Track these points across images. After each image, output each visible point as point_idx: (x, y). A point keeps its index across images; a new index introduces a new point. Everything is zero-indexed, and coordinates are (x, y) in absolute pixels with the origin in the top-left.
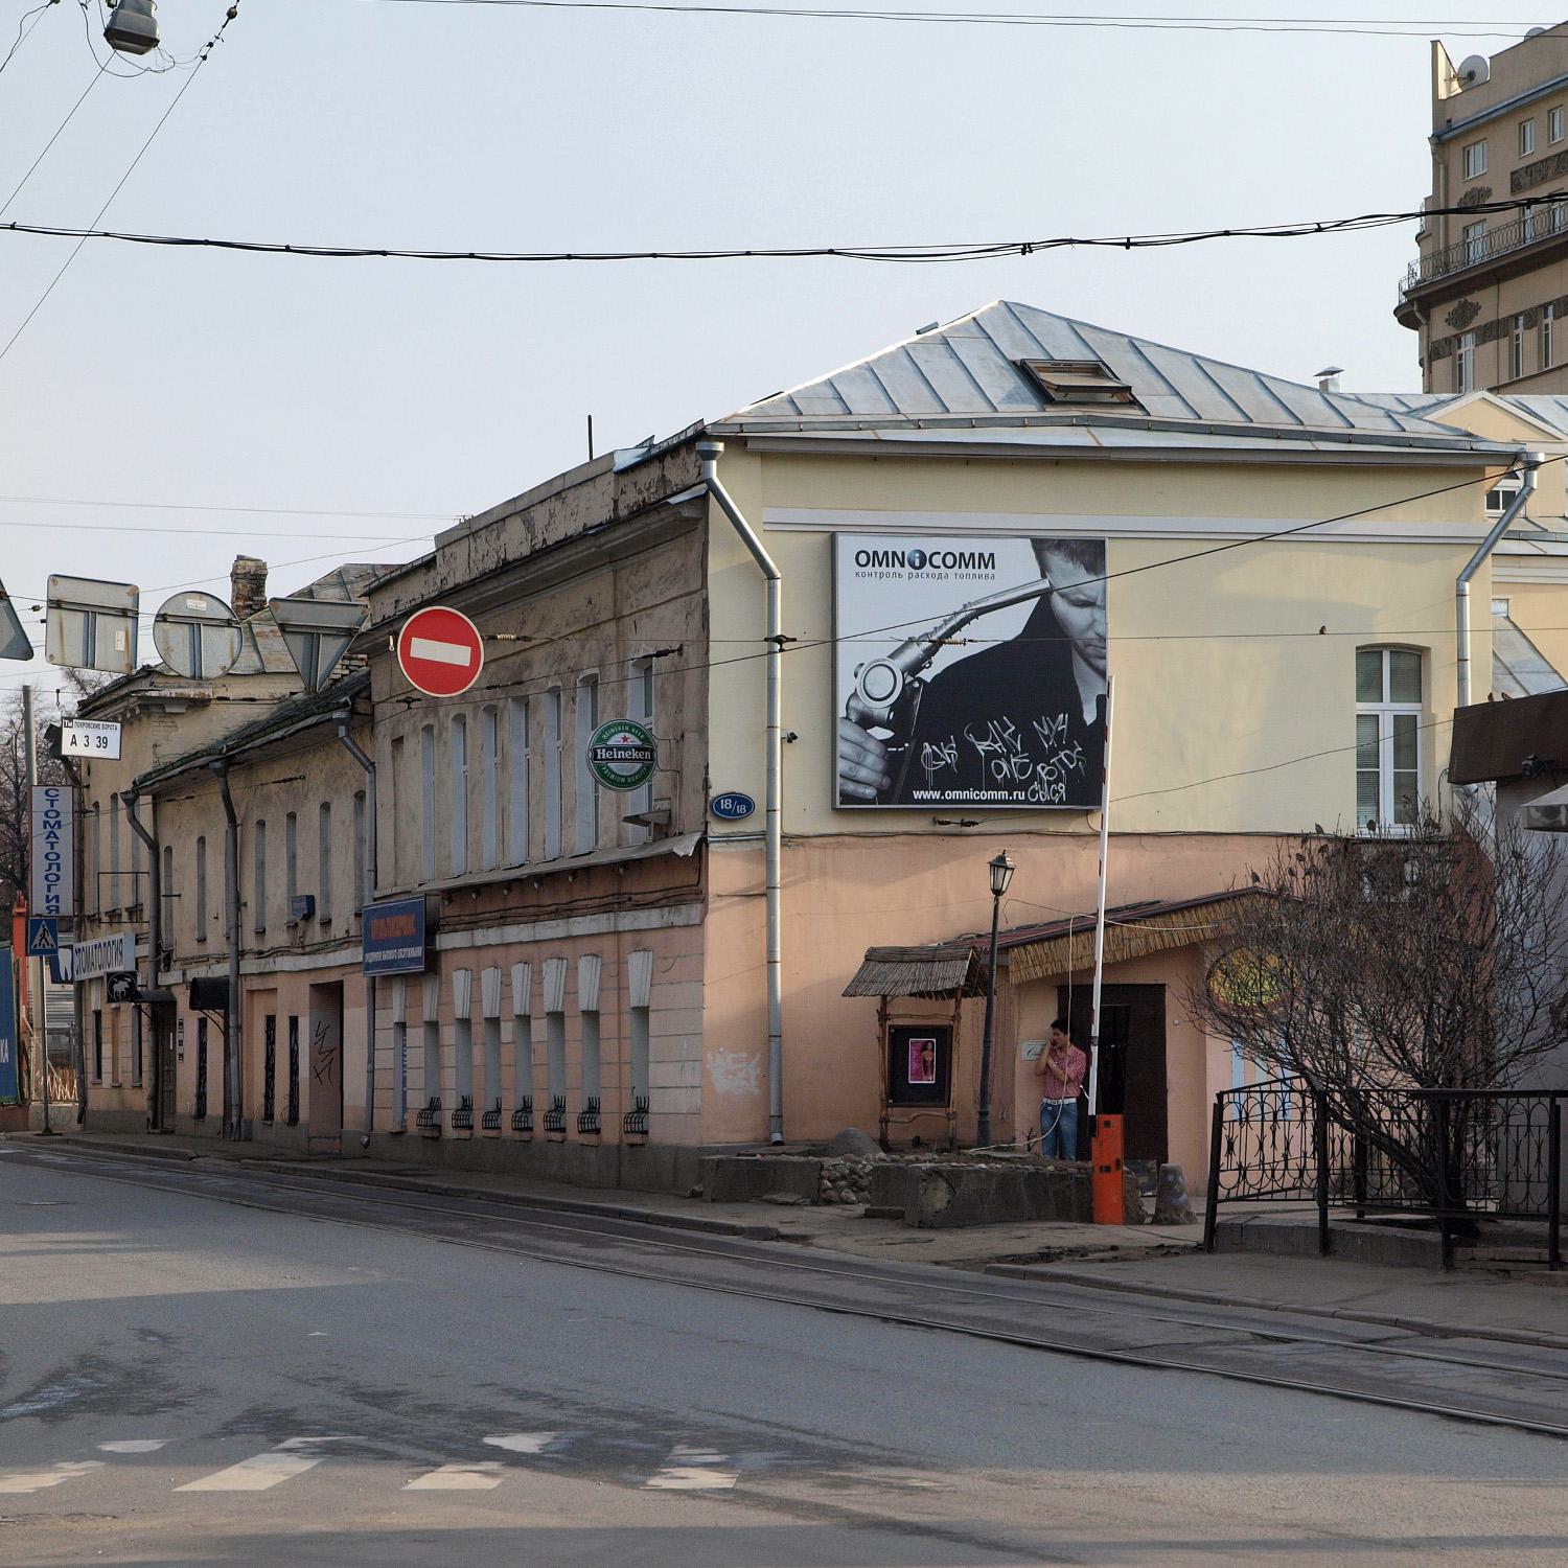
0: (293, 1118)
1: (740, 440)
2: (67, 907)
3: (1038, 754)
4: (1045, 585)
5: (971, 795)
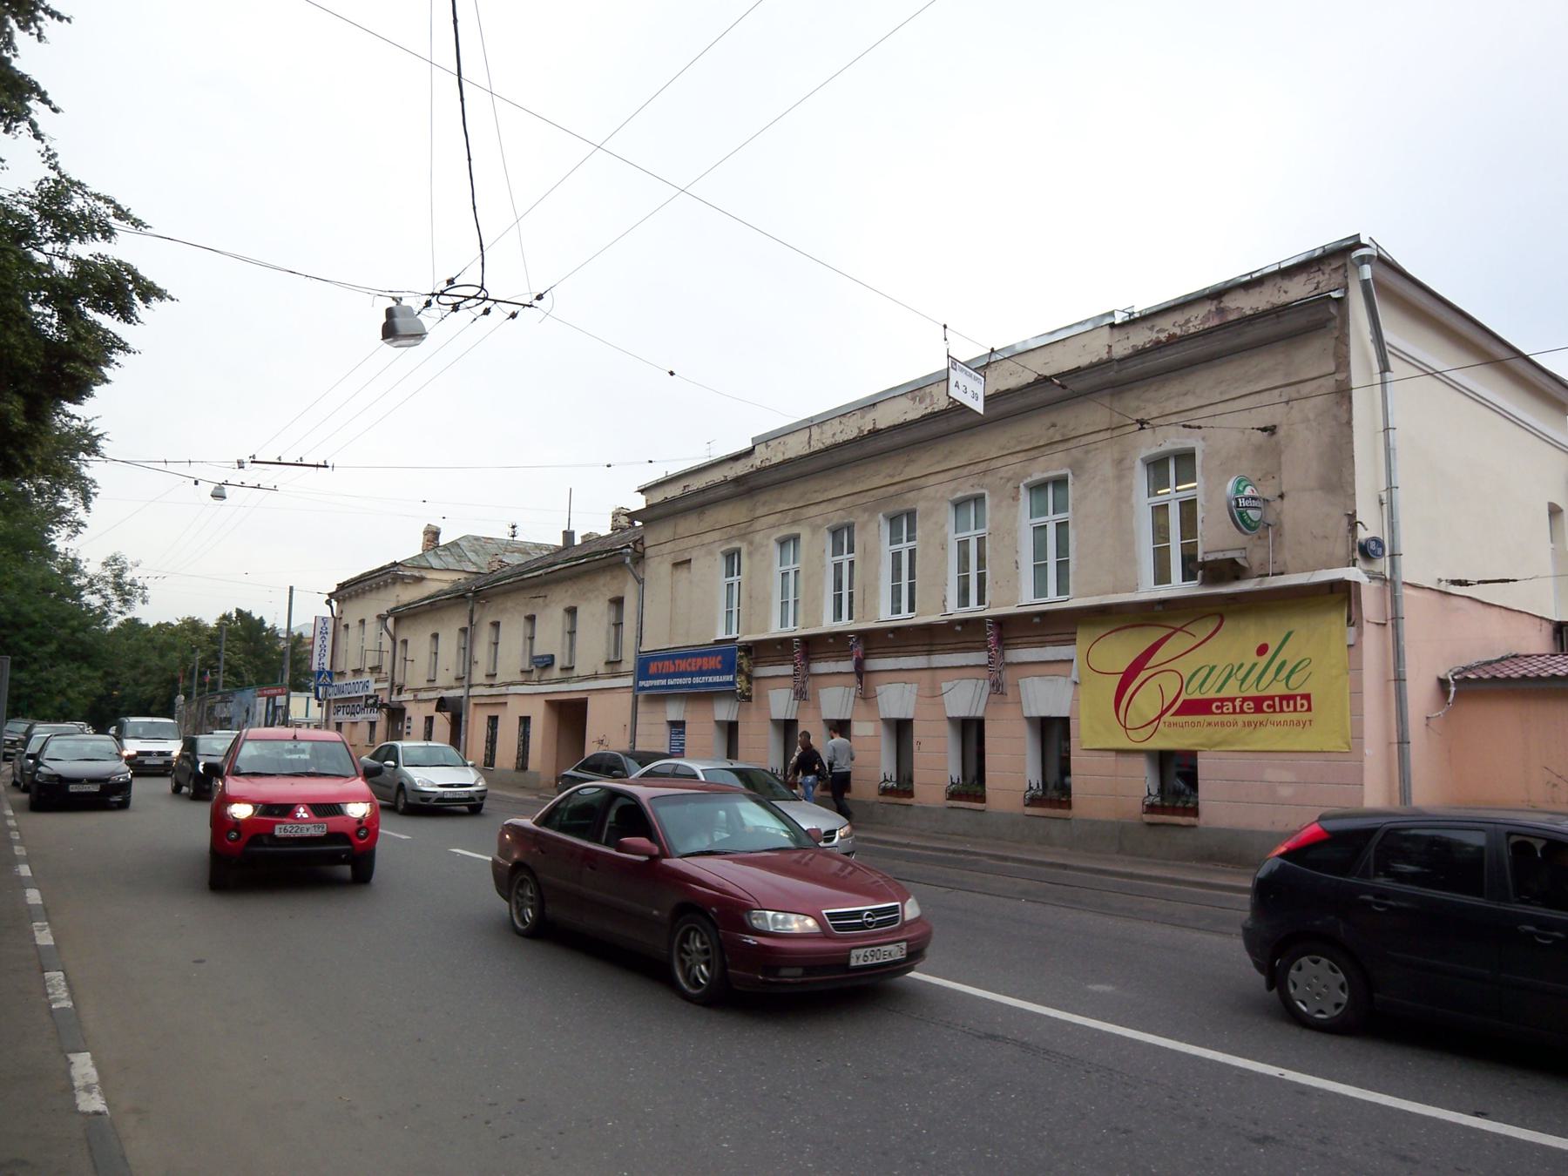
2: (327, 668)
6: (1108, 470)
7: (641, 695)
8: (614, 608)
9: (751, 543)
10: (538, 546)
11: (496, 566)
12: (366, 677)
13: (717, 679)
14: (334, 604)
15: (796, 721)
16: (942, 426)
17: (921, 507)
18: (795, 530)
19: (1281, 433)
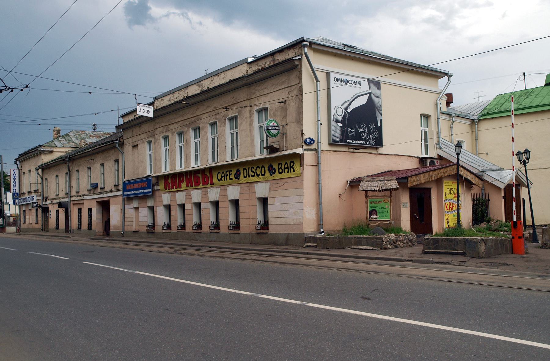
0: (90, 228)
1: (312, 44)
2: (17, 191)
3: (370, 133)
4: (370, 91)
5: (358, 142)
6: (247, 114)
7: (125, 197)
8: (116, 163)
9: (155, 138)
10: (105, 134)
11: (82, 145)
12: (33, 195)
13: (146, 191)
14: (18, 163)
16: (208, 95)
17: (201, 126)
19: (287, 103)
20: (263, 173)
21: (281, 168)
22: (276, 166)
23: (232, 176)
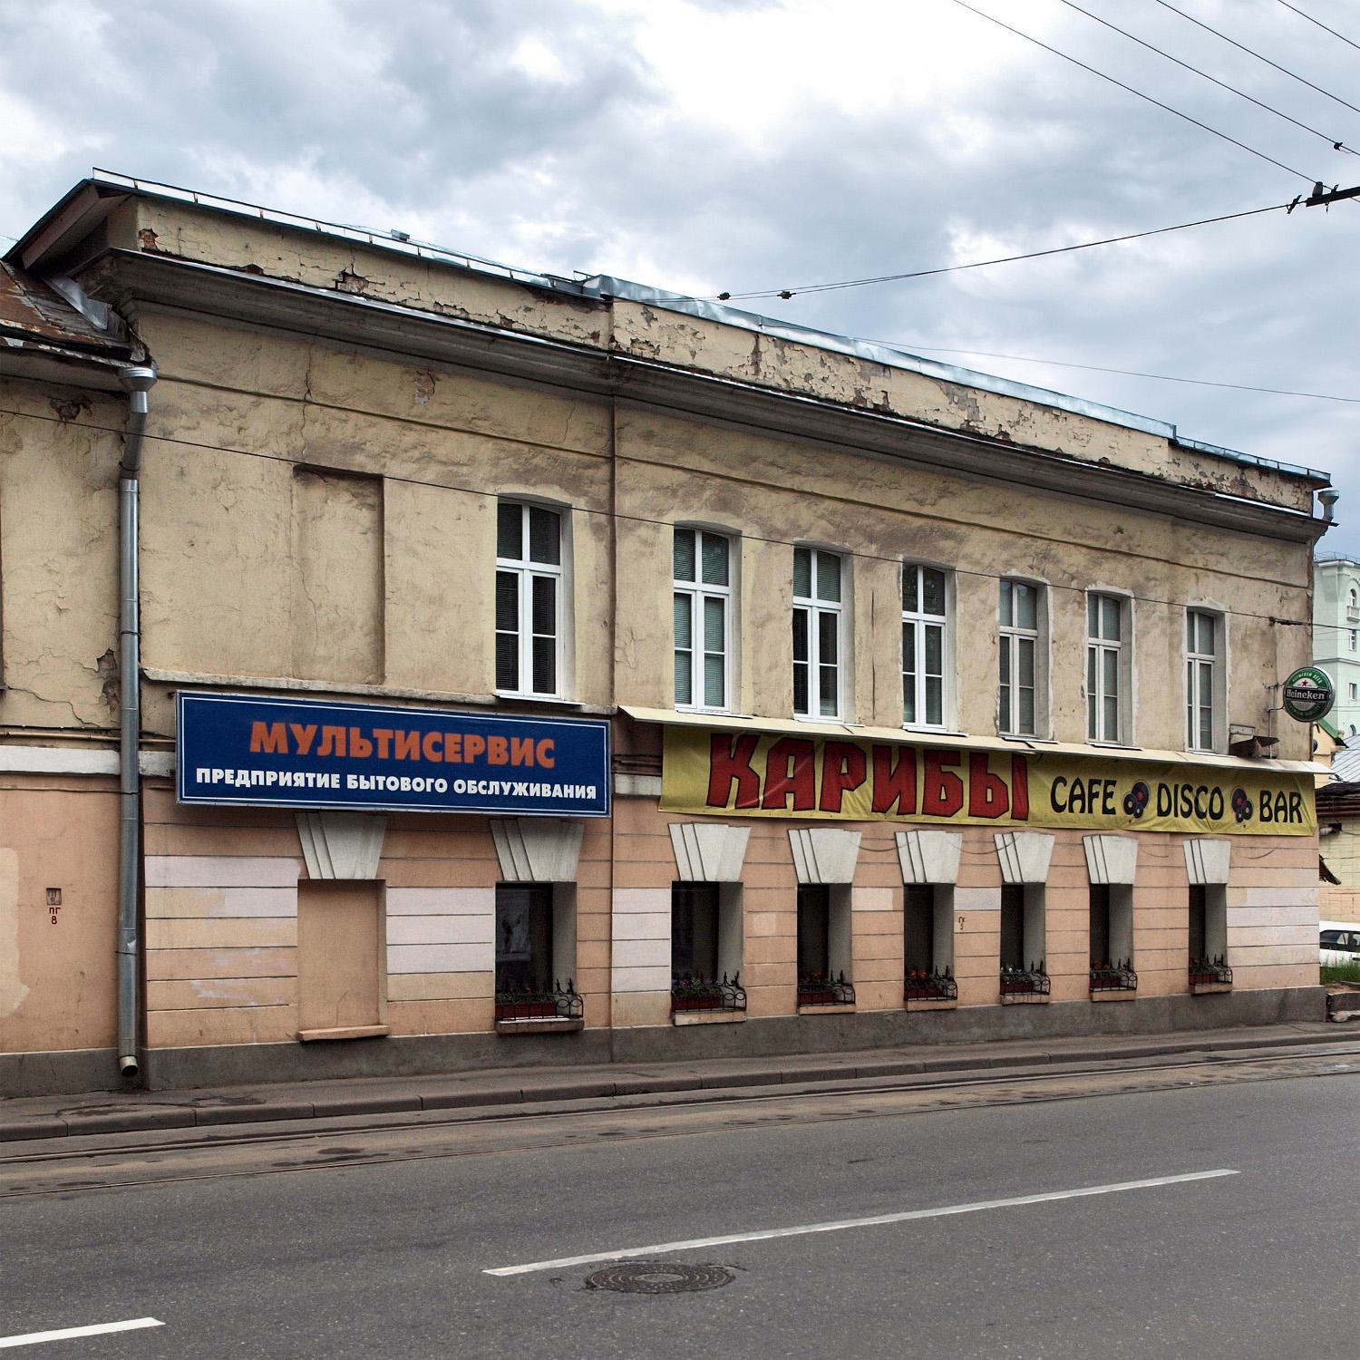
15: (845, 889)
18: (728, 521)
20: (1216, 810)
21: (1267, 805)
22: (1253, 797)
23: (1116, 803)
